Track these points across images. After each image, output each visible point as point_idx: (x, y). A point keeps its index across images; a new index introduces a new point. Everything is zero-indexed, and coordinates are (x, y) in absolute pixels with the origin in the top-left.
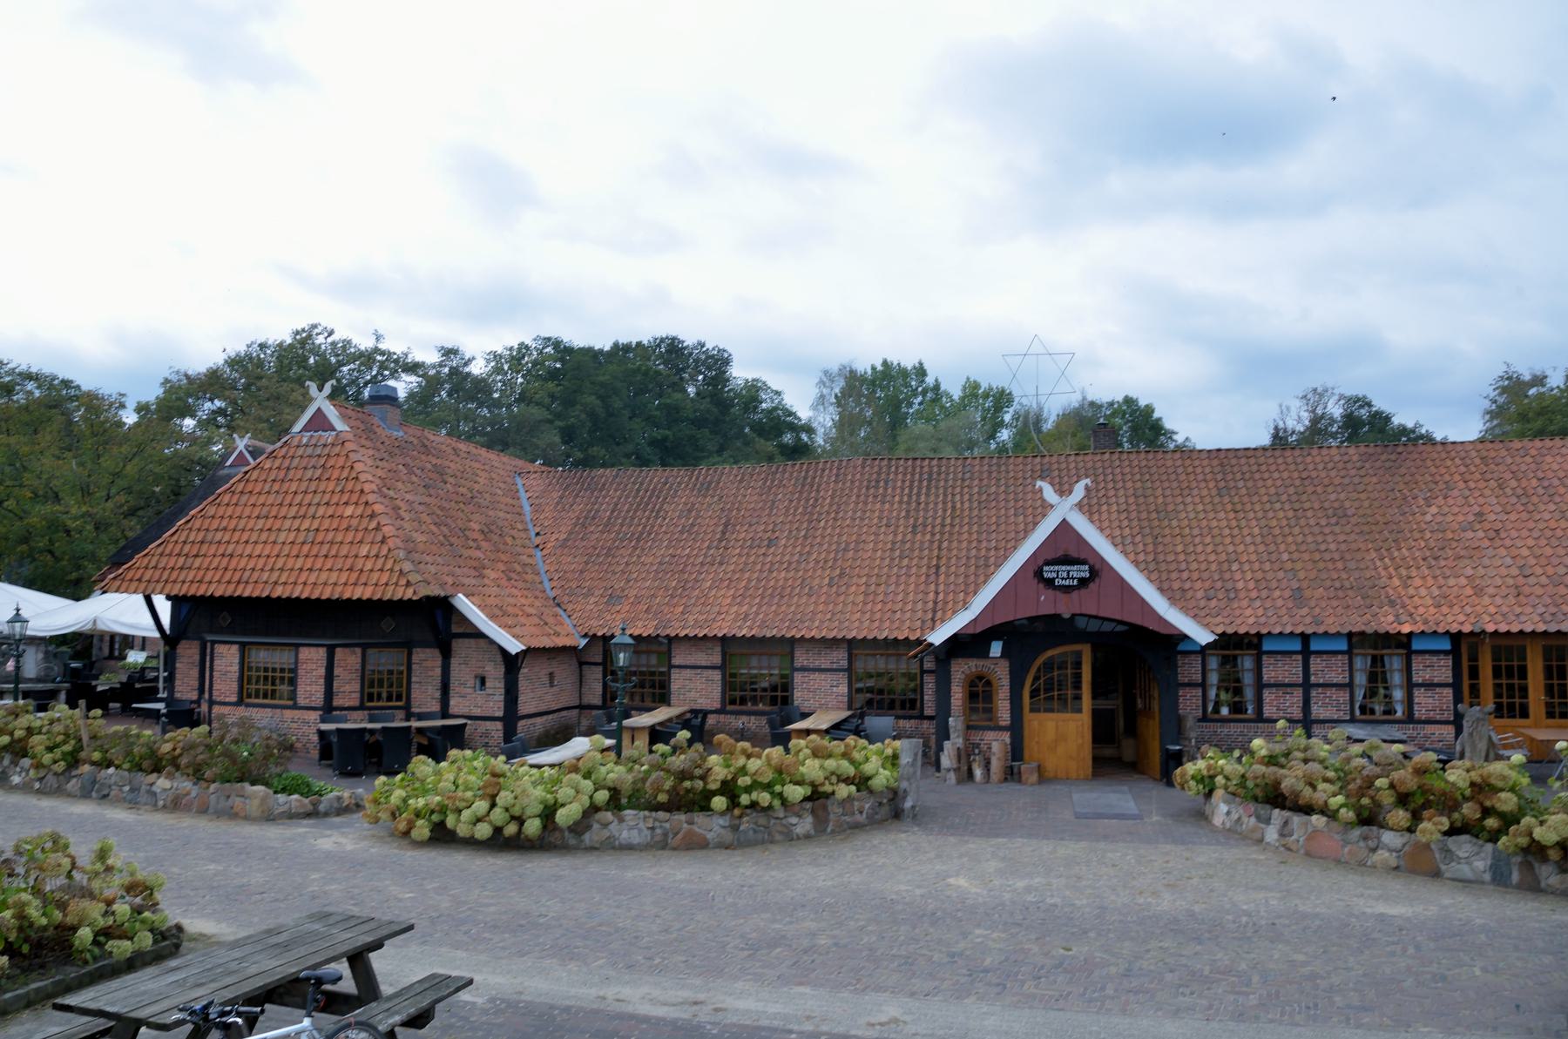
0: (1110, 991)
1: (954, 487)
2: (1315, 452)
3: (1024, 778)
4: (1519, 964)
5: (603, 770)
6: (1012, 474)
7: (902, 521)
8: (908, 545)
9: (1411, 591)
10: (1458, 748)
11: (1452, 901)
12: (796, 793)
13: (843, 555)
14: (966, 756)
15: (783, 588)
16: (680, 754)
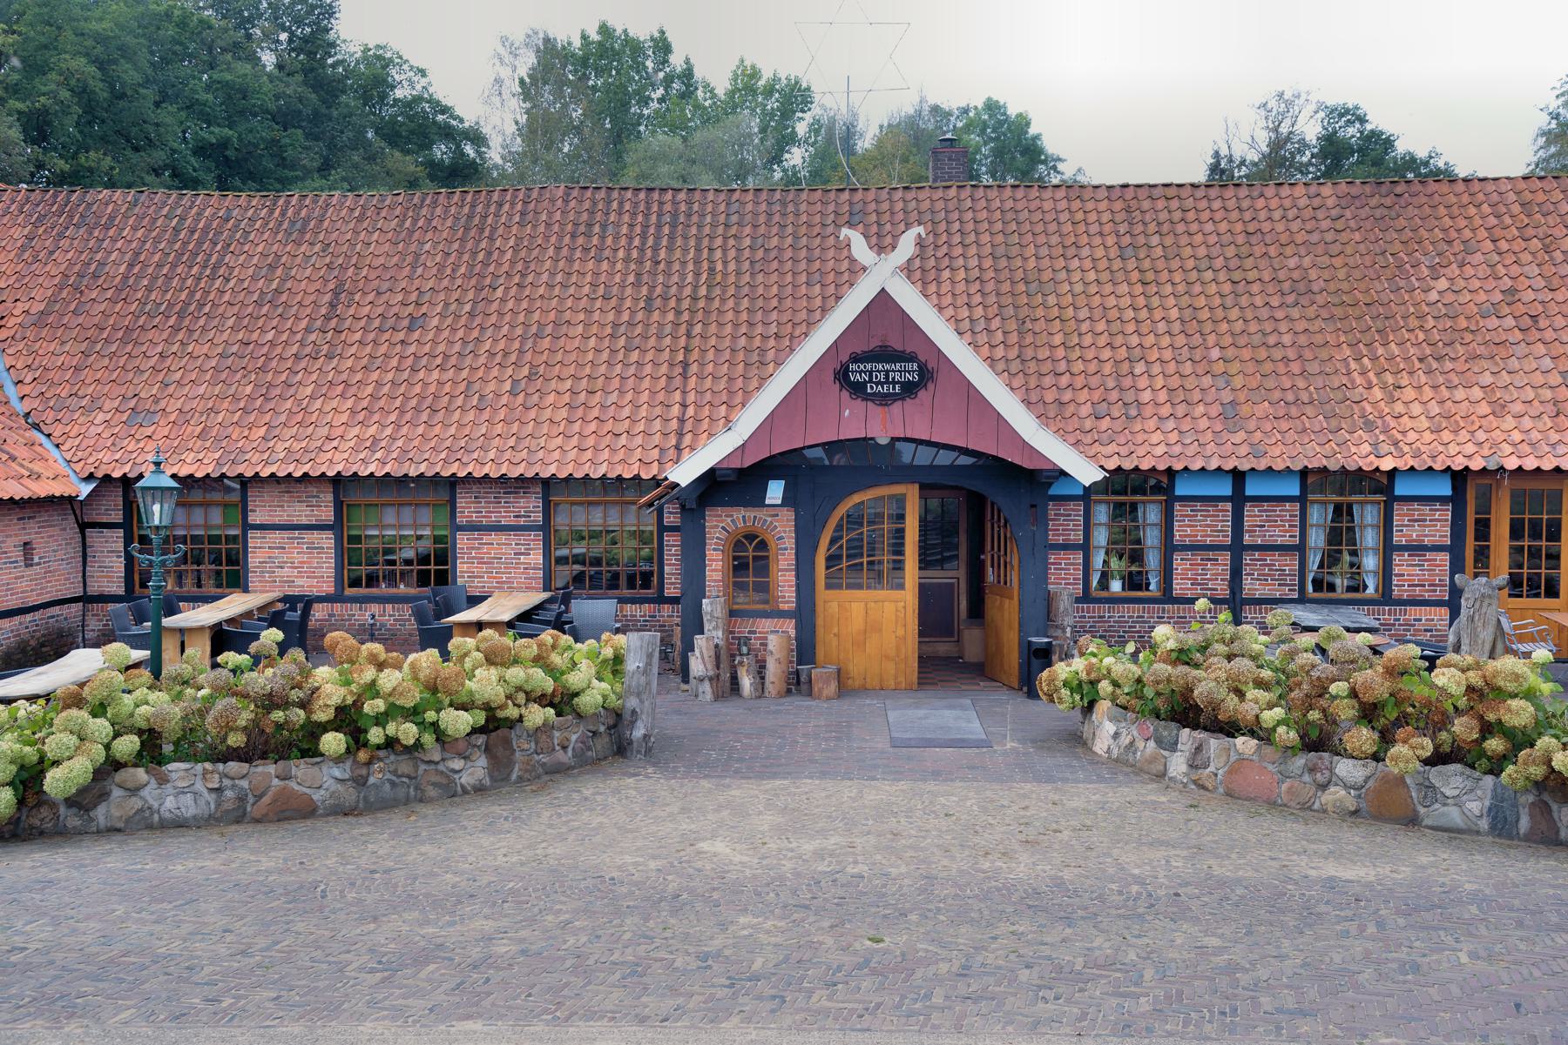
0: (937, 1000)
1: (712, 238)
2: (1270, 191)
3: (816, 689)
4: (1522, 946)
5: (128, 700)
6: (804, 218)
7: (629, 291)
8: (639, 330)
9: (1399, 408)
10: (1451, 638)
11: (1432, 859)
12: (458, 722)
13: (535, 343)
14: (727, 658)
15: (436, 397)
16: (265, 667)
